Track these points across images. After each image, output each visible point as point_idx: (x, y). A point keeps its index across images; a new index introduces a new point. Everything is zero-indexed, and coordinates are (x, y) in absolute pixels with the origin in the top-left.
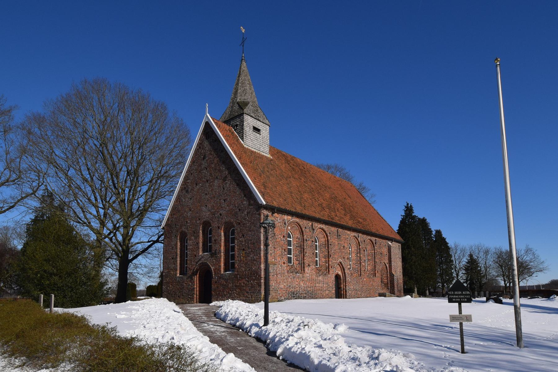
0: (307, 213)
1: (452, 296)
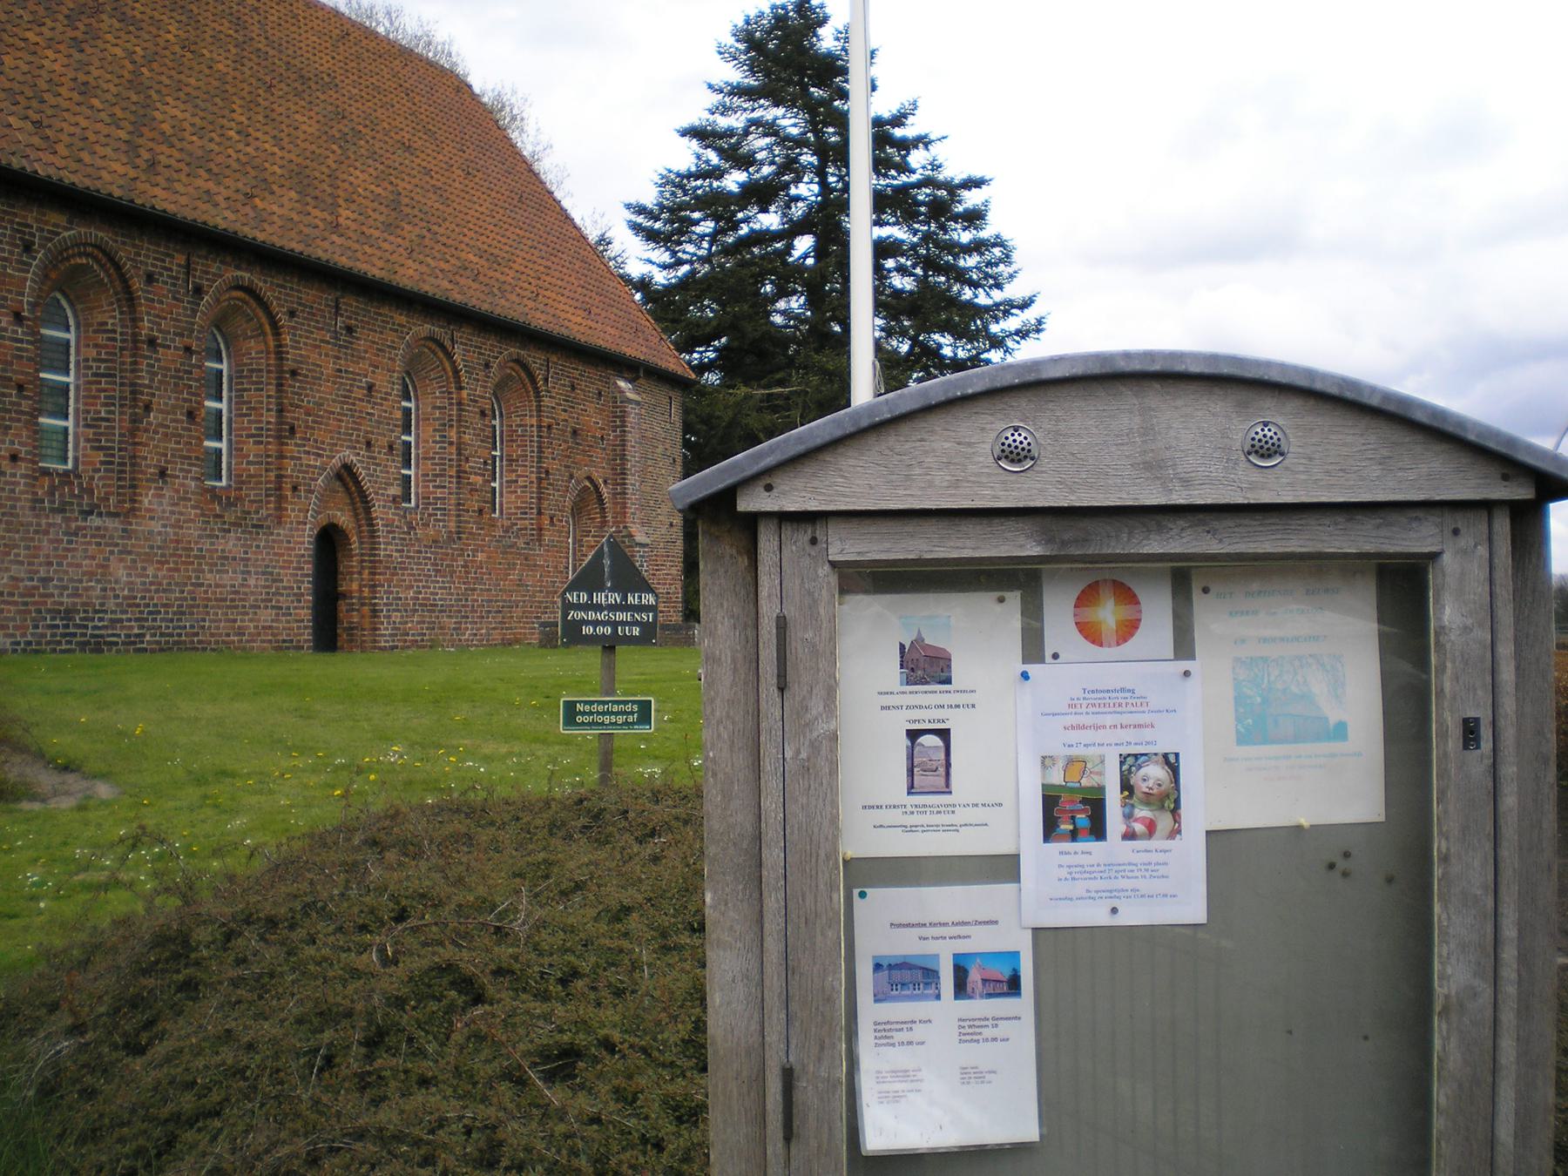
0: (160, 198)
1: (581, 615)
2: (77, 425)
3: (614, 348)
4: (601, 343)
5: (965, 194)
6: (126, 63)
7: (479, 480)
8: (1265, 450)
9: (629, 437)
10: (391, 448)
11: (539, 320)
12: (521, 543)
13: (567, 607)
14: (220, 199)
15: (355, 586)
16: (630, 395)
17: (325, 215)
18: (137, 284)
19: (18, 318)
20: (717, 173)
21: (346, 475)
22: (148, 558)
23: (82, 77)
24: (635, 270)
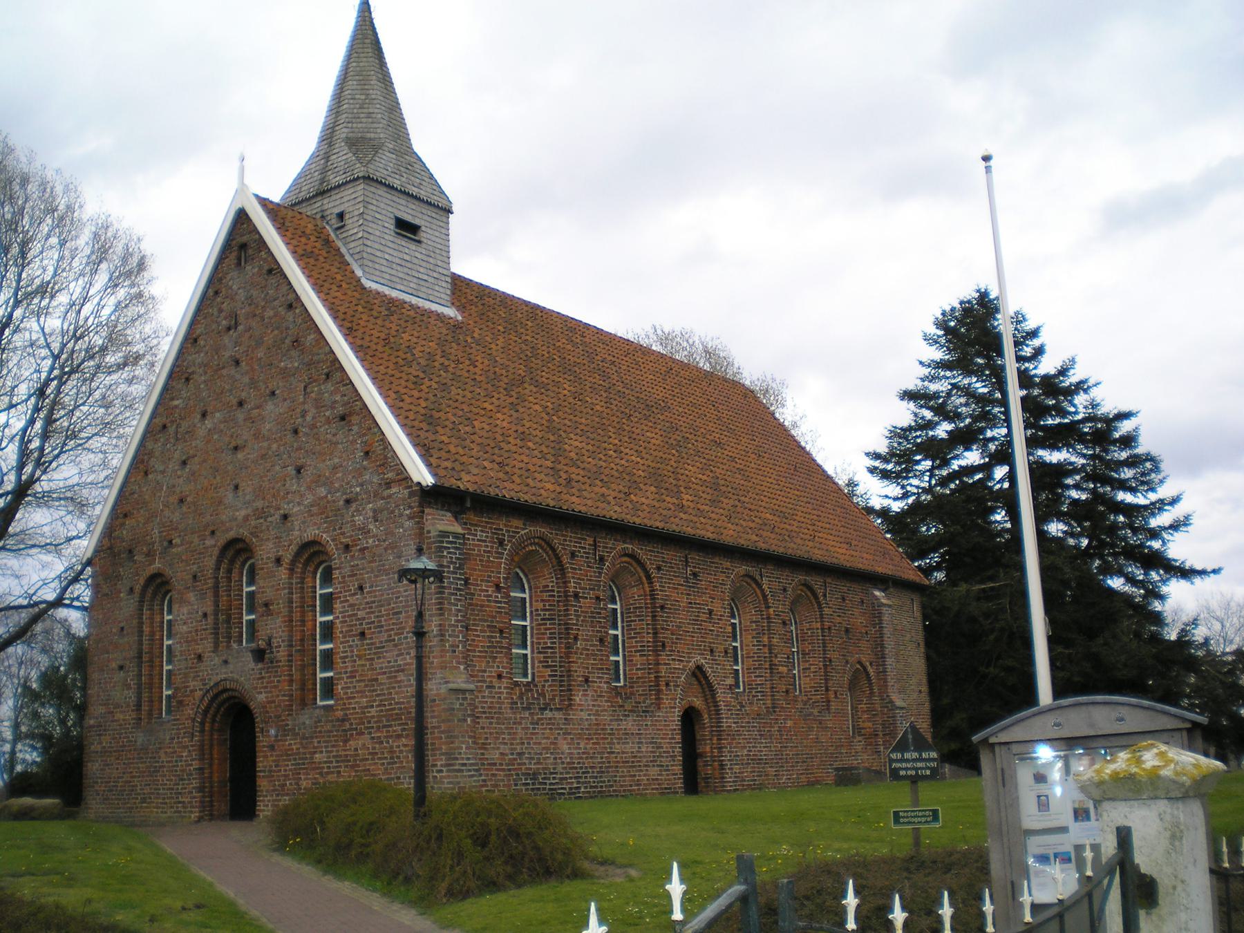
1: (899, 765)
2: (532, 652)
3: (869, 568)
4: (860, 566)
5: (1119, 424)
6: (544, 415)
7: (784, 669)
8: (1122, 719)
9: (885, 630)
10: (726, 652)
11: (818, 555)
12: (815, 712)
13: (892, 761)
14: (610, 499)
15: (708, 748)
16: (884, 601)
17: (674, 500)
18: (566, 559)
19: (498, 588)
20: (930, 425)
21: (698, 673)
22: (580, 736)
23: (521, 429)
24: (877, 503)
